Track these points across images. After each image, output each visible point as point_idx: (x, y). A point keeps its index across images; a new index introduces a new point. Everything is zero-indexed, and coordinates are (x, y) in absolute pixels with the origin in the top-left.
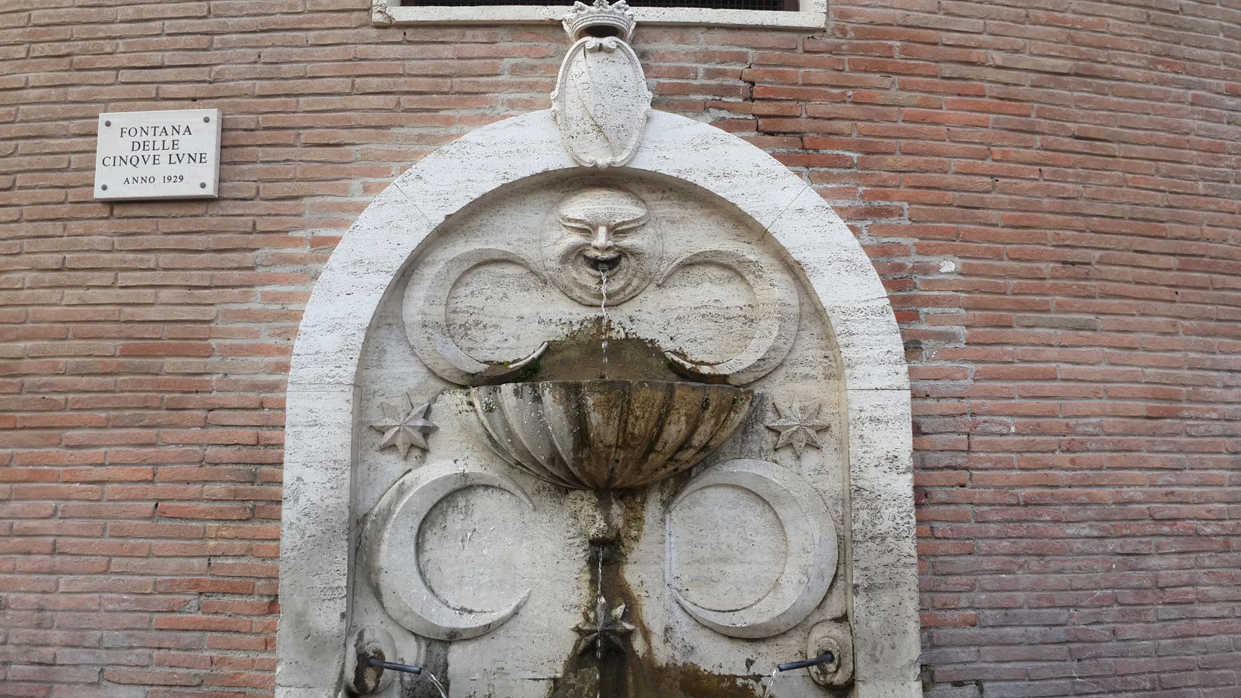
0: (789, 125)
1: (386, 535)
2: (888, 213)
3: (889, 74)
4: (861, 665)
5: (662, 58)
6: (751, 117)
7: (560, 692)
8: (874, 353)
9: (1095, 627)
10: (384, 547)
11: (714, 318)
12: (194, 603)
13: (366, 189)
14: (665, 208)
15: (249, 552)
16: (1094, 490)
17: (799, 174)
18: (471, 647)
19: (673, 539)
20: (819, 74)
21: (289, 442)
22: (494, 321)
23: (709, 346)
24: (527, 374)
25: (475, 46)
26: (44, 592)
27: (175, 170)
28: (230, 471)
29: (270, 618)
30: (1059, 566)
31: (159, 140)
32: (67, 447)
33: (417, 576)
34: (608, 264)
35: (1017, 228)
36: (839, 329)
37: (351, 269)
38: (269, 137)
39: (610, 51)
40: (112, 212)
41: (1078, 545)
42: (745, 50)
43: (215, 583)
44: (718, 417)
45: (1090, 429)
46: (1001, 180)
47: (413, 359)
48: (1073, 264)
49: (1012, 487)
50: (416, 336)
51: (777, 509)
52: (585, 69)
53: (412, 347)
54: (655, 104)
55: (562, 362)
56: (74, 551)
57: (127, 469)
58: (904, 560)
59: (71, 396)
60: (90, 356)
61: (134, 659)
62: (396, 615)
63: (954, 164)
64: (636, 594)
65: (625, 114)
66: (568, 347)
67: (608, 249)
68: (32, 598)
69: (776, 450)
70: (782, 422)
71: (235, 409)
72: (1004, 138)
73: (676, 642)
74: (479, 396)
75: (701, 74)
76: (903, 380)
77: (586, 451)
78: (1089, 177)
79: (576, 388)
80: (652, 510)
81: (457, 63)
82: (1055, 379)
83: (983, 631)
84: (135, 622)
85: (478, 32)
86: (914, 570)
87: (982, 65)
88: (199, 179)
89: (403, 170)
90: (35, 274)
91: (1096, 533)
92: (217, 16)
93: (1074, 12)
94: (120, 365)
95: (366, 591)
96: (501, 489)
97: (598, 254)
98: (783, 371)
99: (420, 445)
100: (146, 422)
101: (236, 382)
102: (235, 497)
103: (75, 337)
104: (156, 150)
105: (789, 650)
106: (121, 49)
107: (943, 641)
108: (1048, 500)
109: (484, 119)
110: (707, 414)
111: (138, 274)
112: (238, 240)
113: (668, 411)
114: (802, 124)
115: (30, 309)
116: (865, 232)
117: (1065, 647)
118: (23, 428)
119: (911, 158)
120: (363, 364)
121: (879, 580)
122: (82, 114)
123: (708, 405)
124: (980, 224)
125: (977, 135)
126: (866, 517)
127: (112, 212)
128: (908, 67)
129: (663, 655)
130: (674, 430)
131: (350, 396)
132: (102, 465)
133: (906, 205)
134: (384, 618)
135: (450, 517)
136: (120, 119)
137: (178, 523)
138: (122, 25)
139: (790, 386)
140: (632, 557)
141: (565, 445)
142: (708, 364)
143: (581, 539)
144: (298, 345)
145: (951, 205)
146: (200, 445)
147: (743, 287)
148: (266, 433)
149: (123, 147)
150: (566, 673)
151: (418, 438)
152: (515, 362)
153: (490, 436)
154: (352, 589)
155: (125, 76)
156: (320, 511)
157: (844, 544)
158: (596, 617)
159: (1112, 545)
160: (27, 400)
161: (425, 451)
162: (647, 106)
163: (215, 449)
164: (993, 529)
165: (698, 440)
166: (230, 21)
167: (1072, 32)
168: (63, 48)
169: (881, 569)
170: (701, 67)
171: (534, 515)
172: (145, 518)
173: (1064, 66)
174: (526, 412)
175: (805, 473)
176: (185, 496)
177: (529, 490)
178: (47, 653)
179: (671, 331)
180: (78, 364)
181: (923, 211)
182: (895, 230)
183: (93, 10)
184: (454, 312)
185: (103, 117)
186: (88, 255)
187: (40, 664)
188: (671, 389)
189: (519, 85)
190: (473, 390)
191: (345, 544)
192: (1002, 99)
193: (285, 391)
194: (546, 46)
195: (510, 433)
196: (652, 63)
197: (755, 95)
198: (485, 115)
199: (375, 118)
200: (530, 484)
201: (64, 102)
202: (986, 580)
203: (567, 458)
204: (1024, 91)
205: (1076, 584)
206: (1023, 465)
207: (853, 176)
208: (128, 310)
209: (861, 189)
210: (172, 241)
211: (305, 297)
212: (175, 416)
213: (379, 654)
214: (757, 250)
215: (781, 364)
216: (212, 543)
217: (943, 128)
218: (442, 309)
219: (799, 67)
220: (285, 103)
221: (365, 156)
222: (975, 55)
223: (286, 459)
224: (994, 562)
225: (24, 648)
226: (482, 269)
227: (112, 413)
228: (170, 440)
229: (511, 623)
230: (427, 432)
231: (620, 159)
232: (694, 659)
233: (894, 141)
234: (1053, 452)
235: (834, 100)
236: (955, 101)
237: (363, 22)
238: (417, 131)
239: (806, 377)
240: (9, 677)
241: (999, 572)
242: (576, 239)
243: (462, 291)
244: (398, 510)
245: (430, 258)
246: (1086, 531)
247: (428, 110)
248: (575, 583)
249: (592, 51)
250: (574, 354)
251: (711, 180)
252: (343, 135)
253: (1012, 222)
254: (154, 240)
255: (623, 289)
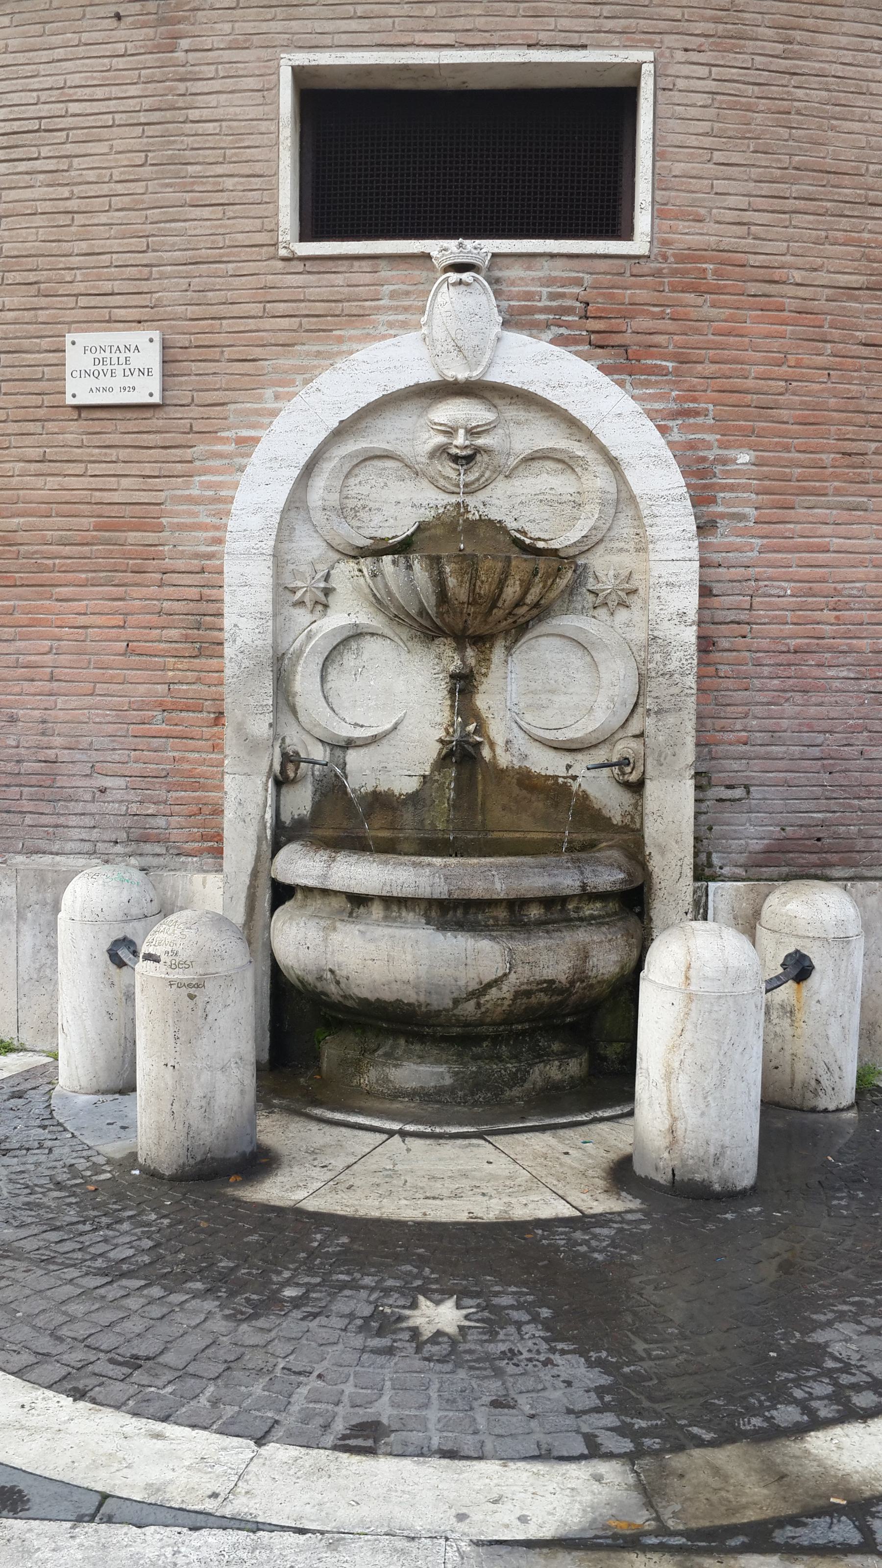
0: (617, 339)
1: (299, 669)
2: (696, 413)
3: (701, 293)
4: (649, 767)
5: (513, 284)
6: (584, 333)
7: (428, 785)
8: (672, 531)
9: (846, 748)
10: (298, 677)
11: (549, 503)
12: (159, 717)
13: (277, 397)
14: (512, 412)
15: (198, 681)
16: (854, 641)
17: (621, 384)
18: (362, 751)
19: (513, 676)
20: (642, 295)
21: (227, 598)
22: (377, 505)
23: (545, 525)
24: (403, 548)
25: (361, 275)
26: (46, 709)
27: (129, 381)
28: (182, 620)
29: (216, 729)
30: (820, 700)
31: (114, 357)
32: (57, 600)
33: (323, 699)
34: (466, 460)
35: (805, 424)
36: (645, 512)
37: (268, 465)
38: (49, 110)
39: (468, 284)
40: (80, 416)
41: (837, 684)
42: (581, 275)
43: (173, 703)
44: (546, 582)
45: (855, 592)
46: (794, 384)
47: (315, 535)
48: (850, 455)
49: (785, 638)
50: (318, 517)
51: (593, 653)
52: (448, 300)
53: (315, 526)
54: (506, 324)
55: (430, 538)
56: (68, 678)
57: (104, 617)
58: (686, 691)
59: (57, 561)
60: (70, 530)
61: (117, 758)
62: (308, 727)
63: (754, 370)
64: (484, 716)
65: (480, 336)
66: (435, 526)
67: (466, 447)
68: (36, 713)
69: (595, 608)
70: (599, 586)
71: (183, 572)
72: (798, 347)
73: (514, 751)
74: (366, 564)
75: (544, 297)
76: (694, 553)
77: (446, 607)
78: (871, 380)
79: (438, 559)
80: (498, 653)
81: (347, 289)
82: (828, 551)
83: (752, 749)
84: (117, 731)
85: (364, 263)
86: (693, 698)
87: (784, 283)
88: (148, 389)
89: (306, 382)
90: (22, 464)
91: (852, 676)
92: (154, 251)
93: (870, 232)
94: (93, 537)
95: (286, 709)
96: (383, 636)
97: (458, 451)
98: (603, 545)
99: (322, 602)
100: (116, 582)
101: (183, 552)
102: (186, 639)
103: (58, 515)
104: (111, 365)
105: (600, 755)
106: (79, 278)
107: (720, 755)
108: (814, 648)
109: (369, 338)
110: (537, 579)
111: (104, 465)
112: (180, 439)
113: (506, 577)
114: (627, 338)
115: (21, 492)
116: (676, 430)
117: (820, 763)
118: (22, 586)
119: (717, 366)
120: (279, 540)
121: (666, 706)
122: (51, 334)
123: (537, 573)
124: (773, 422)
125: (776, 344)
126: (659, 659)
127: (80, 416)
128: (719, 287)
129: (504, 760)
130: (512, 591)
131: (270, 564)
132: (85, 614)
133: (711, 407)
134: (299, 729)
135: (345, 657)
136: (83, 339)
137: (144, 658)
138: (78, 258)
139: (608, 558)
140: (482, 688)
141: (430, 602)
142: (544, 540)
143: (444, 674)
144: (231, 524)
145: (749, 406)
146: (158, 600)
147: (574, 476)
148: (206, 591)
149: (86, 362)
150: (432, 771)
151: (321, 596)
152: (393, 537)
153: (374, 595)
154: (276, 705)
155: (83, 301)
156: (251, 650)
157: (642, 679)
158: (454, 732)
159: (865, 685)
160: (24, 564)
161: (326, 606)
162: (498, 329)
163: (170, 603)
164: (766, 670)
165: (530, 598)
166: (165, 255)
167: (867, 250)
168: (32, 277)
169: (669, 697)
170: (545, 290)
171: (408, 656)
172: (120, 655)
173: (857, 281)
174: (401, 577)
175: (617, 624)
176: (149, 638)
177: (404, 637)
178: (51, 754)
179: (515, 513)
180: (61, 537)
181: (725, 411)
182: (702, 428)
183: (54, 244)
184: (347, 498)
185: (69, 338)
186: (63, 449)
187: (45, 762)
188: (508, 560)
189: (396, 308)
190: (362, 560)
191: (271, 674)
192: (799, 313)
193: (222, 558)
194: (418, 274)
195: (389, 593)
196: (504, 287)
197: (588, 314)
198: (368, 334)
199: (283, 337)
200: (405, 633)
201: (36, 323)
202: (757, 710)
203: (432, 611)
204: (821, 305)
205: (831, 715)
206: (795, 621)
207: (668, 382)
208: (97, 493)
209: (674, 394)
210: (128, 439)
211: (236, 486)
212: (138, 577)
213: (297, 754)
214: (586, 447)
215: (601, 540)
216: (170, 673)
217: (747, 339)
218: (338, 495)
219: (626, 289)
220: (212, 325)
221: (275, 370)
222: (777, 274)
223: (226, 610)
224: (765, 696)
225: (33, 750)
226: (367, 463)
227: (90, 575)
228: (135, 596)
229: (392, 735)
230: (327, 592)
231: (475, 374)
232: (527, 764)
233: (704, 352)
234: (822, 610)
235: (654, 316)
236: (758, 316)
237: (272, 255)
238: (315, 348)
239: (621, 550)
240: (22, 771)
241: (769, 704)
242: (441, 439)
243: (352, 481)
244: (307, 650)
245: (327, 455)
246: (845, 674)
247: (324, 331)
248: (439, 707)
249: (454, 284)
250: (439, 531)
251: (549, 390)
252: (257, 352)
253: (800, 420)
254: (115, 439)
255: (478, 480)
